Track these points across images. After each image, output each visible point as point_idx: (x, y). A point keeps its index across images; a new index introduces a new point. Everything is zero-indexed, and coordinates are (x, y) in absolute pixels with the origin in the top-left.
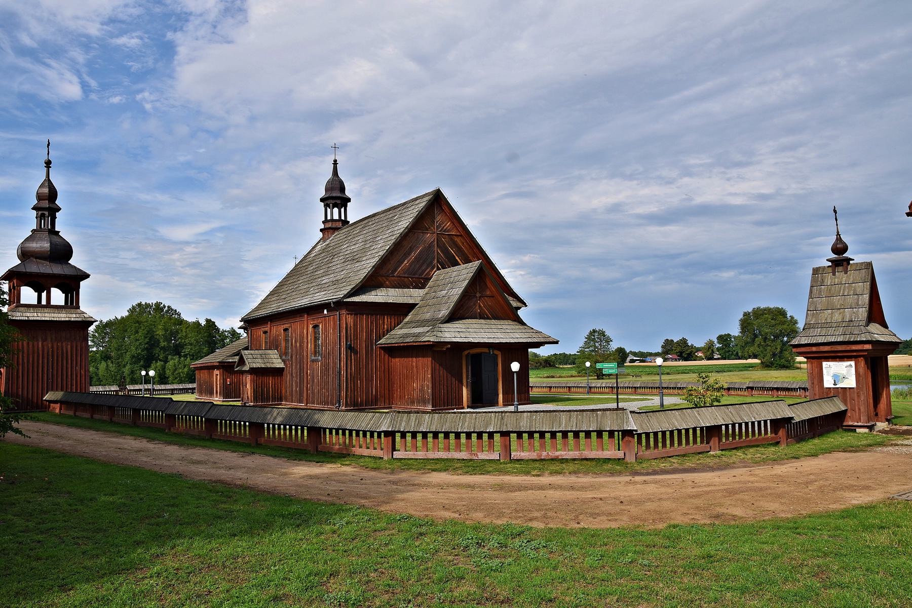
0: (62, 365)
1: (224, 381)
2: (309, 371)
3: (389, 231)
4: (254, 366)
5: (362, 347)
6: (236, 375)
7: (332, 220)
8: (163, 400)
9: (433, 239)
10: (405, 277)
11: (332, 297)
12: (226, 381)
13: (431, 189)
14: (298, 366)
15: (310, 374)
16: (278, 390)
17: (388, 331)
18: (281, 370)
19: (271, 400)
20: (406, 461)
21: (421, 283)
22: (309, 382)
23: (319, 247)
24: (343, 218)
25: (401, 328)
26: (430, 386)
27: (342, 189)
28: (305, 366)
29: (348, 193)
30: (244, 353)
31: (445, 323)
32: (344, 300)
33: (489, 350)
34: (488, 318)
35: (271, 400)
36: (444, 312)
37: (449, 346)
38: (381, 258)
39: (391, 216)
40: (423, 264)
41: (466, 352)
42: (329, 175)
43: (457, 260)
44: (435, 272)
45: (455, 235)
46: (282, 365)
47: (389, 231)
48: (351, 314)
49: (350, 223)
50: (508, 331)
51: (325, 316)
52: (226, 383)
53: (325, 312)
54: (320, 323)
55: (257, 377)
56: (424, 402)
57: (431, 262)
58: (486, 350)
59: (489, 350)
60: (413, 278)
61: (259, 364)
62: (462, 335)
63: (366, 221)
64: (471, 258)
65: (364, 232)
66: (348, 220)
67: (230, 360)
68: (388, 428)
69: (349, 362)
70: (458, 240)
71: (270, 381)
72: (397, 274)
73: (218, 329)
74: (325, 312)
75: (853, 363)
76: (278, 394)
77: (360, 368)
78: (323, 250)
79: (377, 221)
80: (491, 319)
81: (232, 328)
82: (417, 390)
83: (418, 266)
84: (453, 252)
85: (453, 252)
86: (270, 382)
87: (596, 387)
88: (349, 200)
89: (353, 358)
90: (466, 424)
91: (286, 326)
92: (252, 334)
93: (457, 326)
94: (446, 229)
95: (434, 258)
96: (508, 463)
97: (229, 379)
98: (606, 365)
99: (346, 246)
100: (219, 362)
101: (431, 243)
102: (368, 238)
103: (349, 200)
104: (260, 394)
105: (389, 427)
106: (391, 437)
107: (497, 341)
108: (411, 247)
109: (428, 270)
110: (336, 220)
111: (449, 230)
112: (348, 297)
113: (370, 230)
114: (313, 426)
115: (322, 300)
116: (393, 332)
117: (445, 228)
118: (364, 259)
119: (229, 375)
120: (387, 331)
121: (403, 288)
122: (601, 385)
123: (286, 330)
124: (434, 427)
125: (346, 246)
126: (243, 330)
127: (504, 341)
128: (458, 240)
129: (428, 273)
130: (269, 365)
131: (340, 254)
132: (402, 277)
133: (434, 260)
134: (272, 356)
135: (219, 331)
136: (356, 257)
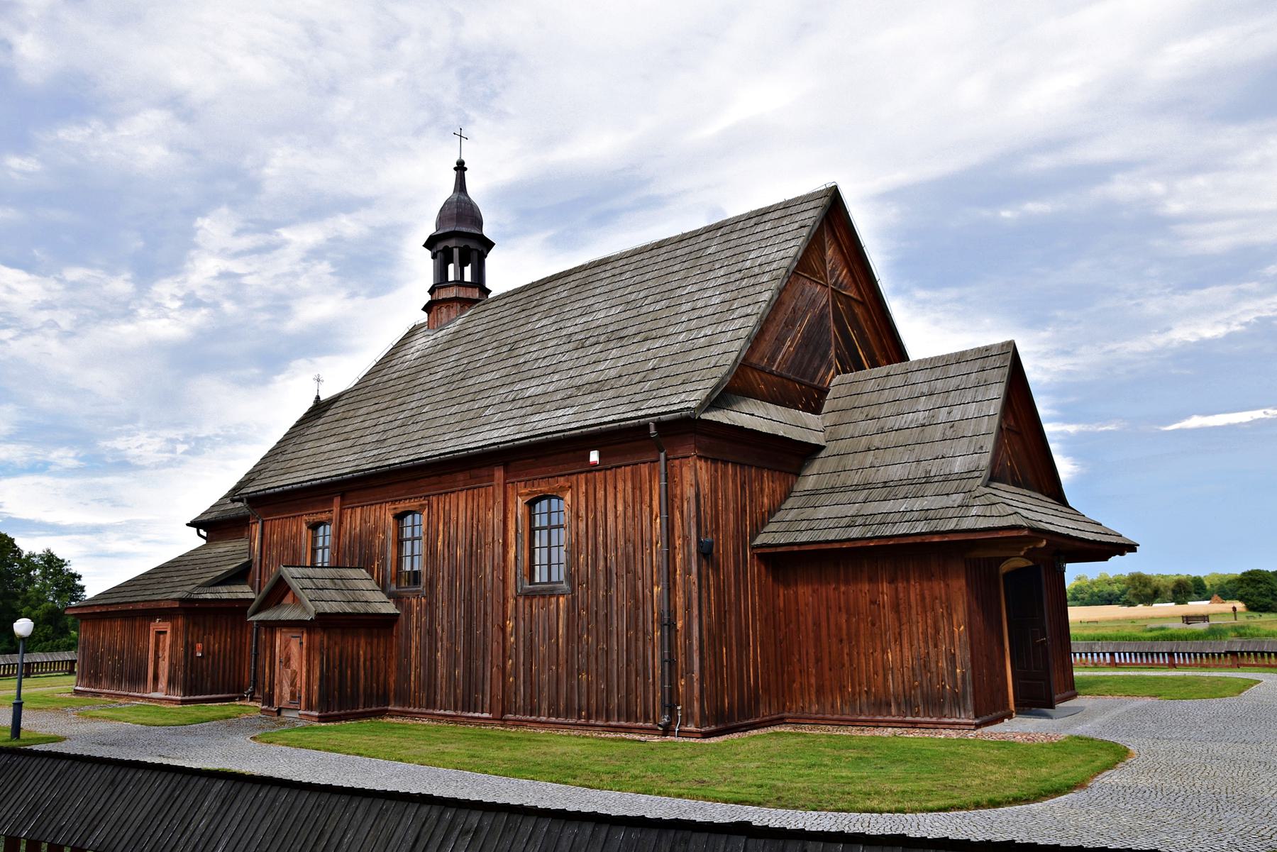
0: (332, 833)
1: (189, 648)
2: (510, 624)
4: (327, 608)
5: (725, 548)
6: (218, 633)
8: (408, 823)
9: (825, 300)
12: (194, 649)
13: (815, 183)
16: (378, 677)
17: (772, 513)
18: (390, 620)
19: (362, 700)
20: (160, 721)
21: (812, 400)
30: (291, 573)
32: (703, 416)
35: (362, 700)
38: (762, 317)
42: (447, 189)
44: (833, 377)
46: (390, 608)
48: (706, 459)
51: (594, 468)
52: (194, 653)
53: (594, 457)
55: (329, 638)
56: (957, 702)
61: (334, 605)
63: (530, 293)
64: (878, 358)
67: (209, 596)
69: (704, 595)
71: (361, 648)
73: (18, 552)
74: (594, 457)
76: (378, 686)
77: (725, 612)
81: (48, 551)
83: (807, 357)
86: (361, 652)
87: (1152, 654)
88: (489, 245)
91: (401, 507)
95: (830, 345)
97: (199, 645)
100: (181, 600)
103: (489, 245)
104: (337, 686)
106: (450, 280)
110: (467, 285)
111: (846, 285)
112: (707, 411)
114: (828, 832)
119: (196, 629)
120: (769, 512)
122: (1242, 647)
123: (400, 517)
128: (858, 310)
129: (823, 380)
130: (361, 608)
133: (829, 349)
134: (360, 584)
135: (20, 555)
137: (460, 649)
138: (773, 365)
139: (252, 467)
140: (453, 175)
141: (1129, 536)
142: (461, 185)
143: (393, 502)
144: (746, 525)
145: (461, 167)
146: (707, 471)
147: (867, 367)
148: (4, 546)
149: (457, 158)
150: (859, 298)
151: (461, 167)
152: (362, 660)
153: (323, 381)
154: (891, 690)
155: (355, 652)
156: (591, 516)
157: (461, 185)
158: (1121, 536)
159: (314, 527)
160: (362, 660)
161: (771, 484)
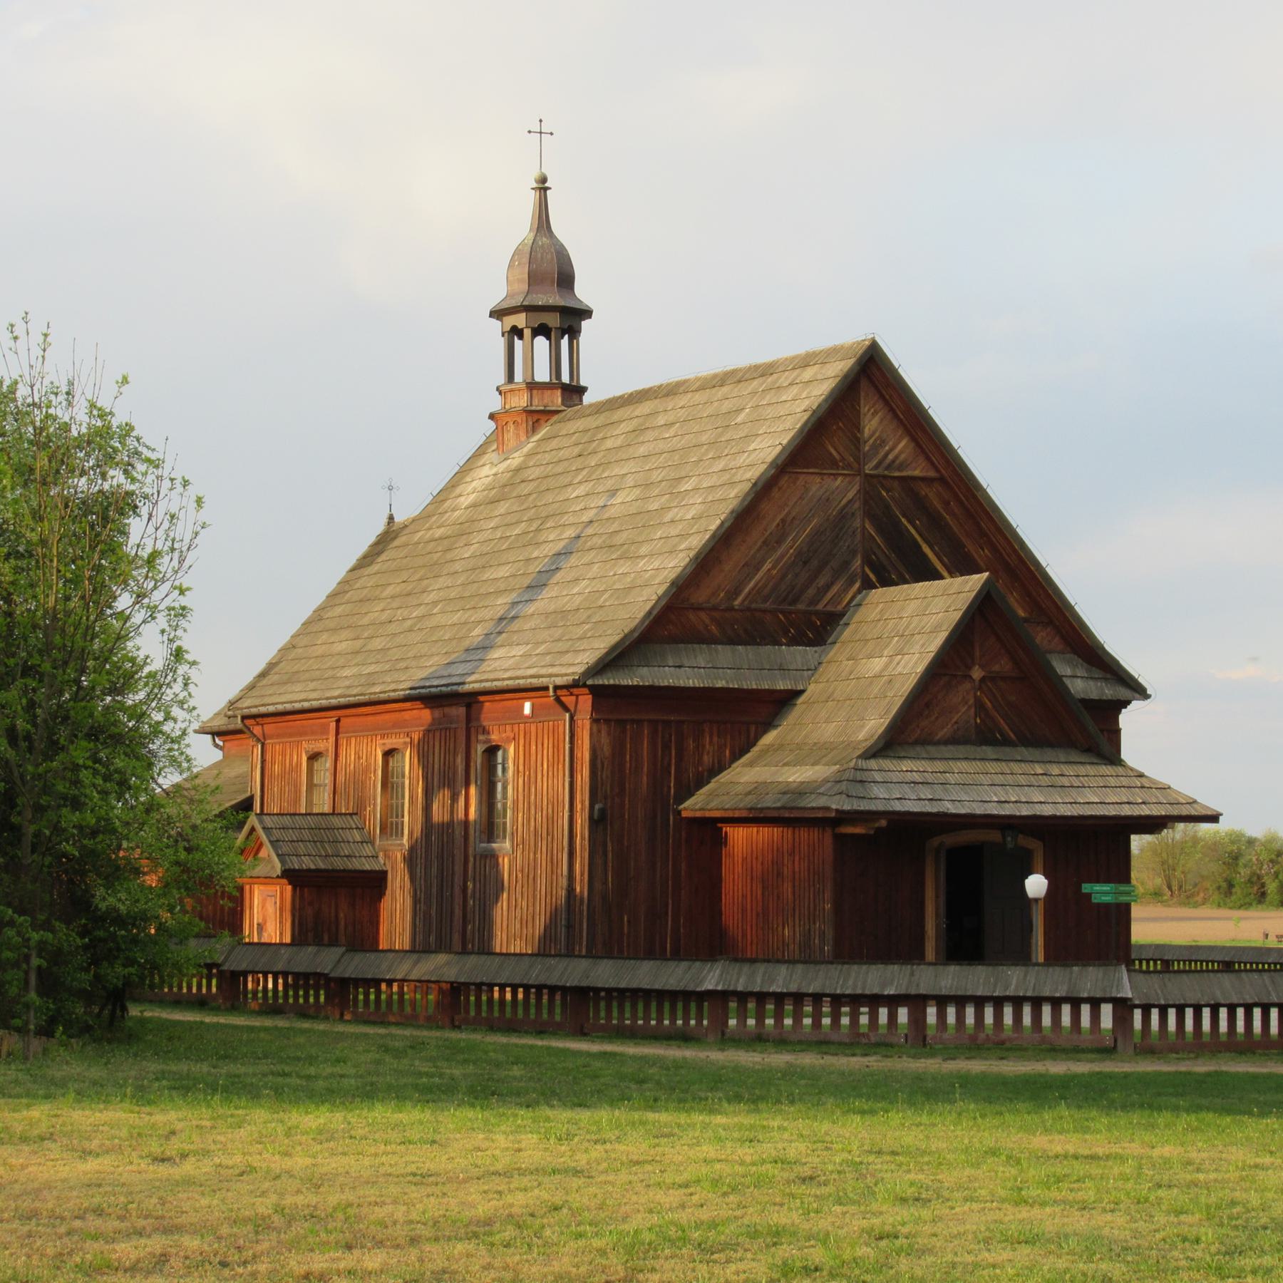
2: (470, 885)
3: (720, 465)
7: (532, 386)
10: (764, 611)
11: (551, 670)
14: (434, 870)
15: (474, 891)
22: (469, 916)
23: (486, 471)
24: (565, 378)
25: (751, 764)
26: (830, 935)
27: (566, 279)
28: (458, 868)
29: (584, 292)
31: (869, 758)
33: (1004, 837)
34: (1006, 742)
36: (874, 724)
37: (883, 823)
39: (726, 406)
40: (819, 571)
41: (936, 841)
42: (521, 229)
43: (925, 555)
45: (923, 479)
47: (720, 465)
49: (588, 399)
50: (1065, 781)
53: (527, 708)
54: (508, 740)
57: (846, 564)
58: (995, 836)
59: (1004, 837)
60: (790, 613)
62: (926, 793)
65: (642, 450)
66: (583, 383)
68: (716, 985)
70: (932, 495)
72: (744, 601)
74: (527, 708)
75: (278, 888)
78: (502, 491)
79: (682, 414)
80: (1017, 746)
82: (791, 947)
84: (913, 531)
85: (913, 531)
89: (520, 815)
90: (851, 982)
92: (268, 757)
93: (906, 765)
94: (893, 461)
96: (919, 1039)
98: (1097, 887)
99: (581, 490)
101: (846, 505)
102: (656, 476)
105: (717, 984)
107: (1025, 811)
108: (783, 521)
109: (835, 589)
113: (661, 445)
115: (519, 673)
116: (724, 777)
117: (891, 457)
118: (644, 550)
121: (759, 644)
124: (796, 986)
125: (581, 490)
126: (209, 737)
127: (1047, 811)
130: (339, 864)
131: (565, 519)
132: (755, 610)
136: (619, 539)
137: (433, 912)
138: (736, 599)
139: (288, 638)
140: (531, 198)
141: (1209, 801)
142: (543, 222)
143: (383, 737)
144: (670, 787)
145: (542, 186)
146: (609, 734)
147: (945, 574)
148: (1278, 1251)
149: (535, 174)
150: (932, 474)
151: (542, 186)
152: (342, 923)
153: (398, 489)
154: (740, 944)
155: (333, 915)
156: (527, 773)
157: (543, 222)
158: (1195, 802)
159: (313, 757)
160: (342, 923)
161: (715, 739)
